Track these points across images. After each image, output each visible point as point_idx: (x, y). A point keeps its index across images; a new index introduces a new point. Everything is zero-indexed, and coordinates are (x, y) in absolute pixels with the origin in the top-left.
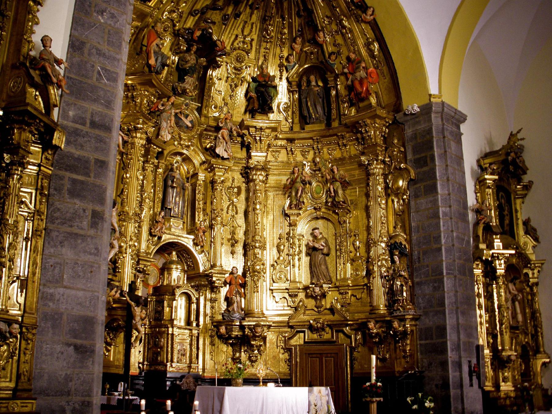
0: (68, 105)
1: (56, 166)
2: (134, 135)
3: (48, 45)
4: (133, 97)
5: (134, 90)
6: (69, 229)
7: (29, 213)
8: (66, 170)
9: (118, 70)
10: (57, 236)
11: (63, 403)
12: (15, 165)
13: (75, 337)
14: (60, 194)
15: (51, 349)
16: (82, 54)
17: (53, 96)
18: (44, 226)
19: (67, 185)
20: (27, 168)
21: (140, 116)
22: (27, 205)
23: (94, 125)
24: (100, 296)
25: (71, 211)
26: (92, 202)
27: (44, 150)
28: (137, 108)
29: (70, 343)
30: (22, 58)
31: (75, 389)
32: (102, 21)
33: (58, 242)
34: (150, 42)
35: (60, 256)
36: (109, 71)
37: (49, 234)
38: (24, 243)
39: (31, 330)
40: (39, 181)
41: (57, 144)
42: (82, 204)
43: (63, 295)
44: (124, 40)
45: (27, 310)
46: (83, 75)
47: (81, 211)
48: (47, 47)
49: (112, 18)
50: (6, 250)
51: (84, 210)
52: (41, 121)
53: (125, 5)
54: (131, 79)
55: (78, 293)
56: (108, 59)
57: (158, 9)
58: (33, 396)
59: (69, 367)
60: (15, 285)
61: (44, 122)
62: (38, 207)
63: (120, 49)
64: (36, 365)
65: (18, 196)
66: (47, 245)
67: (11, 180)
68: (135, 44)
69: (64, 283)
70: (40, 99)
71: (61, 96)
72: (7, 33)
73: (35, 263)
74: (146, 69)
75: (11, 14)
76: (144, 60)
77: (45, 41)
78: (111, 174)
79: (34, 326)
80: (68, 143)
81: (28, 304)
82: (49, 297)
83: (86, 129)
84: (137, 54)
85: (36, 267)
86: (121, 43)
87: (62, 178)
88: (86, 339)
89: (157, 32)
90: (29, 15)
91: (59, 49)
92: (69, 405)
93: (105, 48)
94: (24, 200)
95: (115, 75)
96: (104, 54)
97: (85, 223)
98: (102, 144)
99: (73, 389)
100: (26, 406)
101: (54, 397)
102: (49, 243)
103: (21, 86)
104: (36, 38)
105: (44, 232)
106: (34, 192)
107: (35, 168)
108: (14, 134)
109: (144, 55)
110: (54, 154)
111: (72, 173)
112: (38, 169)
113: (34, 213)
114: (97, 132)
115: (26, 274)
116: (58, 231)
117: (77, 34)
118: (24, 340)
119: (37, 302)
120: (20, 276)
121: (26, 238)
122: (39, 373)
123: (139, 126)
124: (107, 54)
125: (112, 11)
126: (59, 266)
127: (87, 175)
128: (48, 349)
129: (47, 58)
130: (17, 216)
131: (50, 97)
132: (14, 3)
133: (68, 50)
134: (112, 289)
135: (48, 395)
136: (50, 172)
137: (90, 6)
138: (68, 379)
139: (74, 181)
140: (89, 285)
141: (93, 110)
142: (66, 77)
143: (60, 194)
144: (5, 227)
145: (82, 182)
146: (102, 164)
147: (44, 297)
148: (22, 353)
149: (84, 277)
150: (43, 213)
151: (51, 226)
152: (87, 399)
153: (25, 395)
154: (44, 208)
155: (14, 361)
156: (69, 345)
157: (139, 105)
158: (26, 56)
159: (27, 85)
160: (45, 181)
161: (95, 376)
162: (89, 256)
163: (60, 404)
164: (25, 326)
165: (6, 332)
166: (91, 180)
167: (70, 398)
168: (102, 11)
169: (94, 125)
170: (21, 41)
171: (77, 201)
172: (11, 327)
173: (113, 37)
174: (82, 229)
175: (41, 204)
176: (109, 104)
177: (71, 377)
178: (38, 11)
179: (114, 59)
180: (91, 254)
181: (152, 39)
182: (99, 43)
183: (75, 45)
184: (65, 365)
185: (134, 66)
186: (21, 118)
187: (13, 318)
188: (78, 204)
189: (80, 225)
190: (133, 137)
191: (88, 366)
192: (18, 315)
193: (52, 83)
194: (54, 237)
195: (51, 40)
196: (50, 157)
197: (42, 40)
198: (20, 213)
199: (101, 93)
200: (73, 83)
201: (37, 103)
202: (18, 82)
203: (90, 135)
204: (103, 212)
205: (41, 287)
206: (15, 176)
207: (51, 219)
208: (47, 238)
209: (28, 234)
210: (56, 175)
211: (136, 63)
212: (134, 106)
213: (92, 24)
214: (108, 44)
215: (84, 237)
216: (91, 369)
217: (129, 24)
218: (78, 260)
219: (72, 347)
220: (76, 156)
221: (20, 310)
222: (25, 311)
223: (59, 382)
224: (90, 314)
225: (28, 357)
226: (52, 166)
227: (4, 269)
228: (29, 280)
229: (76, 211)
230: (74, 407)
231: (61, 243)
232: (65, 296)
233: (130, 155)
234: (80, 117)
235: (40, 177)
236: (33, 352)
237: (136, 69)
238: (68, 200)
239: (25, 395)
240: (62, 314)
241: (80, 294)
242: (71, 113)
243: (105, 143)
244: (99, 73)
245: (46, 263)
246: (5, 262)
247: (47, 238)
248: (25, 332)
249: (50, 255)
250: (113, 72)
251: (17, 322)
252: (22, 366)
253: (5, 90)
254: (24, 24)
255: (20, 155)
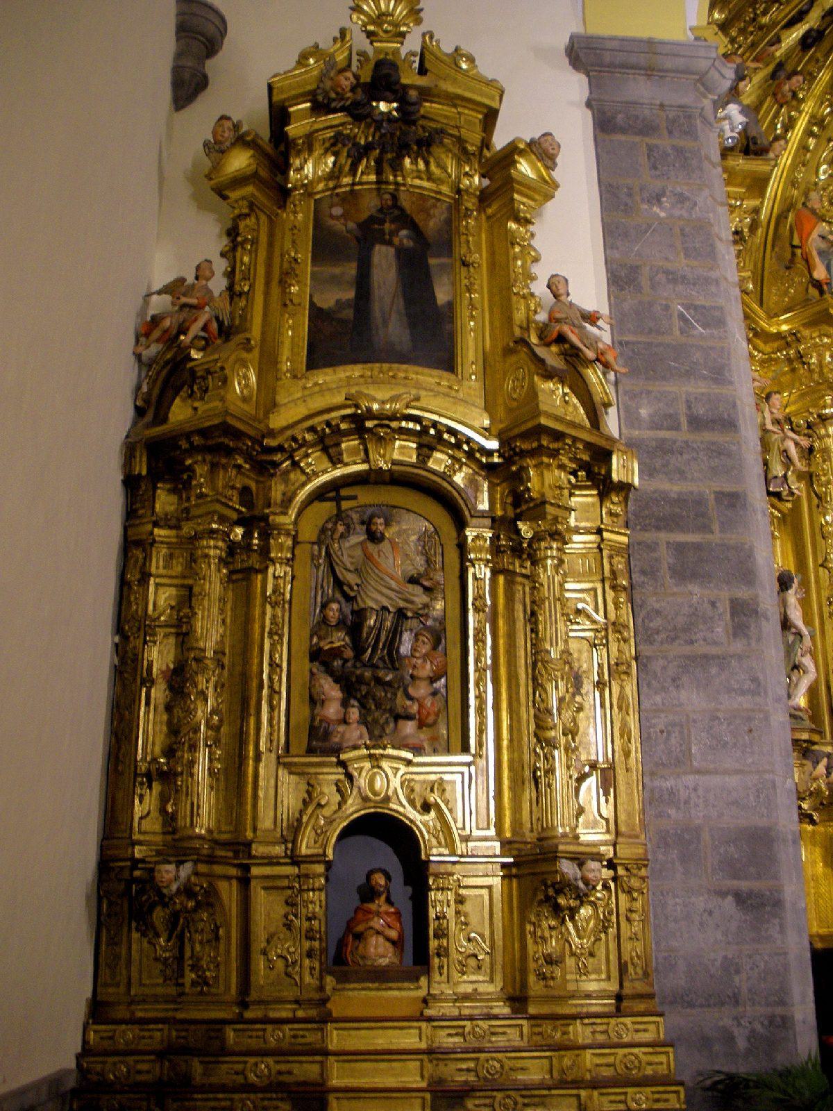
0: (633, 396)
1: (636, 525)
2: (823, 432)
3: (562, 291)
4: (800, 356)
5: (798, 340)
6: (687, 650)
7: (597, 631)
8: (658, 528)
9: (721, 302)
10: (664, 668)
11: (727, 1022)
12: (543, 539)
13: (735, 877)
14: (656, 580)
15: (685, 906)
16: (639, 289)
17: (599, 389)
18: (633, 652)
19: (666, 558)
20: (571, 541)
21: (825, 390)
22: (588, 617)
23: (696, 423)
24: (779, 780)
25: (686, 610)
26: (728, 583)
27: (603, 496)
28: (816, 376)
29: (724, 889)
30: (517, 332)
31: (750, 990)
32: (663, 214)
33: (669, 680)
34: (804, 236)
35: (678, 709)
36: (704, 307)
37: (646, 666)
38: (597, 694)
39: (635, 871)
40: (605, 561)
41: (624, 480)
42: (706, 592)
43: (695, 790)
44: (721, 240)
45: (623, 829)
46: (650, 331)
47: (707, 606)
48: (560, 295)
49: (682, 202)
50: (555, 711)
51: (713, 604)
52: (575, 439)
53: (701, 169)
54: (786, 321)
55: (727, 779)
56: (694, 284)
57: (804, 165)
58: (659, 1009)
59: (729, 943)
60: (592, 782)
61: (582, 440)
62: (612, 616)
63: (714, 259)
64: (657, 943)
65: (562, 600)
66: (644, 689)
67: (541, 570)
68: (777, 249)
69: (695, 764)
70: (575, 401)
71: (616, 383)
72: (481, 294)
73: (625, 731)
74: (814, 292)
75: (480, 257)
76: (802, 275)
77: (556, 286)
78: (759, 516)
79: (642, 862)
80: (646, 471)
81: (622, 817)
82: (666, 797)
83: (684, 435)
84: (788, 268)
85: (629, 740)
86: (712, 246)
87: (652, 547)
88: (759, 876)
89: (813, 212)
90: (513, 248)
91: (589, 291)
92: (739, 1024)
93: (681, 264)
94: (580, 606)
95: (717, 314)
96: (684, 277)
97: (720, 630)
98: (724, 458)
99: (744, 990)
100: (645, 1030)
101: (706, 1010)
102: (649, 685)
103: (526, 384)
104: (539, 288)
105: (634, 663)
106: (599, 586)
107: (592, 538)
108: (529, 480)
109: (800, 265)
110: (626, 499)
111: (672, 531)
112: (599, 540)
113: (606, 630)
114: (707, 436)
115: (610, 756)
116: (665, 658)
117: (617, 256)
118: (623, 891)
119: (643, 811)
120: (597, 761)
121: (598, 682)
122: (665, 958)
123: (827, 411)
124: (690, 276)
125: (678, 190)
126: (677, 729)
127: (706, 528)
128: (679, 908)
129: (563, 316)
130: (566, 642)
131: (593, 390)
132: (484, 236)
133: (609, 291)
134: (818, 763)
135: (691, 1005)
136: (625, 539)
137: (630, 195)
138: (731, 967)
139: (680, 548)
140: (750, 760)
141: (688, 394)
142: (616, 345)
143: (656, 580)
144: (546, 668)
145: (698, 547)
146: (733, 501)
147: (653, 800)
148: (622, 919)
149: (735, 744)
150: (627, 627)
151: (646, 650)
152: (779, 1010)
153: (641, 1007)
154: (626, 615)
155: (610, 937)
156: (722, 894)
157: (817, 370)
158: (525, 325)
159: (536, 378)
160: (616, 559)
161: (791, 957)
162: (740, 699)
163: (721, 1023)
164: (621, 864)
165: (576, 880)
166: (716, 537)
167: (741, 1009)
168: (657, 195)
169: (696, 423)
170: (509, 300)
171: (695, 588)
172: (584, 868)
173: (695, 238)
174: (715, 643)
175: (617, 607)
176: (719, 374)
177: (737, 964)
178: (533, 235)
179: (707, 281)
180: (743, 693)
181: (807, 227)
182: (667, 259)
183: (621, 278)
184: (719, 937)
185: (786, 293)
186: (535, 445)
187: (588, 850)
188: (696, 592)
189: (709, 635)
190: (820, 438)
191: (771, 936)
192: (605, 843)
193: (588, 363)
194: (658, 670)
195: (567, 281)
196: (618, 509)
197: (549, 287)
198: (571, 634)
199: (698, 356)
200: (633, 350)
201: (570, 409)
202: (520, 377)
203: (695, 446)
204: (755, 599)
205: (646, 780)
206: (549, 562)
207: (644, 635)
208: (642, 675)
209: (600, 674)
210: (639, 544)
211: (789, 287)
212: (807, 374)
213: (644, 226)
214: (687, 256)
215: (722, 661)
216: (779, 942)
217: (722, 204)
218: (718, 710)
219: (730, 898)
220: (674, 496)
221: (608, 831)
222: (617, 833)
223: (711, 976)
224: (762, 822)
225: (637, 927)
226: (627, 527)
227: (556, 753)
228: (617, 769)
229: (696, 609)
230: (753, 1031)
231: (674, 680)
232: (700, 792)
233: (825, 475)
234: (665, 415)
235: (605, 553)
236: (647, 916)
237: (792, 299)
238: (675, 589)
239: (641, 1007)
240: (698, 829)
241: (733, 781)
242: (644, 412)
243: (729, 455)
244: (681, 316)
245: (649, 727)
246: (555, 738)
247: (642, 675)
248: (622, 876)
249: (655, 711)
250: (712, 307)
251: (598, 857)
252: (627, 946)
253: (500, 401)
254: (508, 266)
255: (549, 517)
